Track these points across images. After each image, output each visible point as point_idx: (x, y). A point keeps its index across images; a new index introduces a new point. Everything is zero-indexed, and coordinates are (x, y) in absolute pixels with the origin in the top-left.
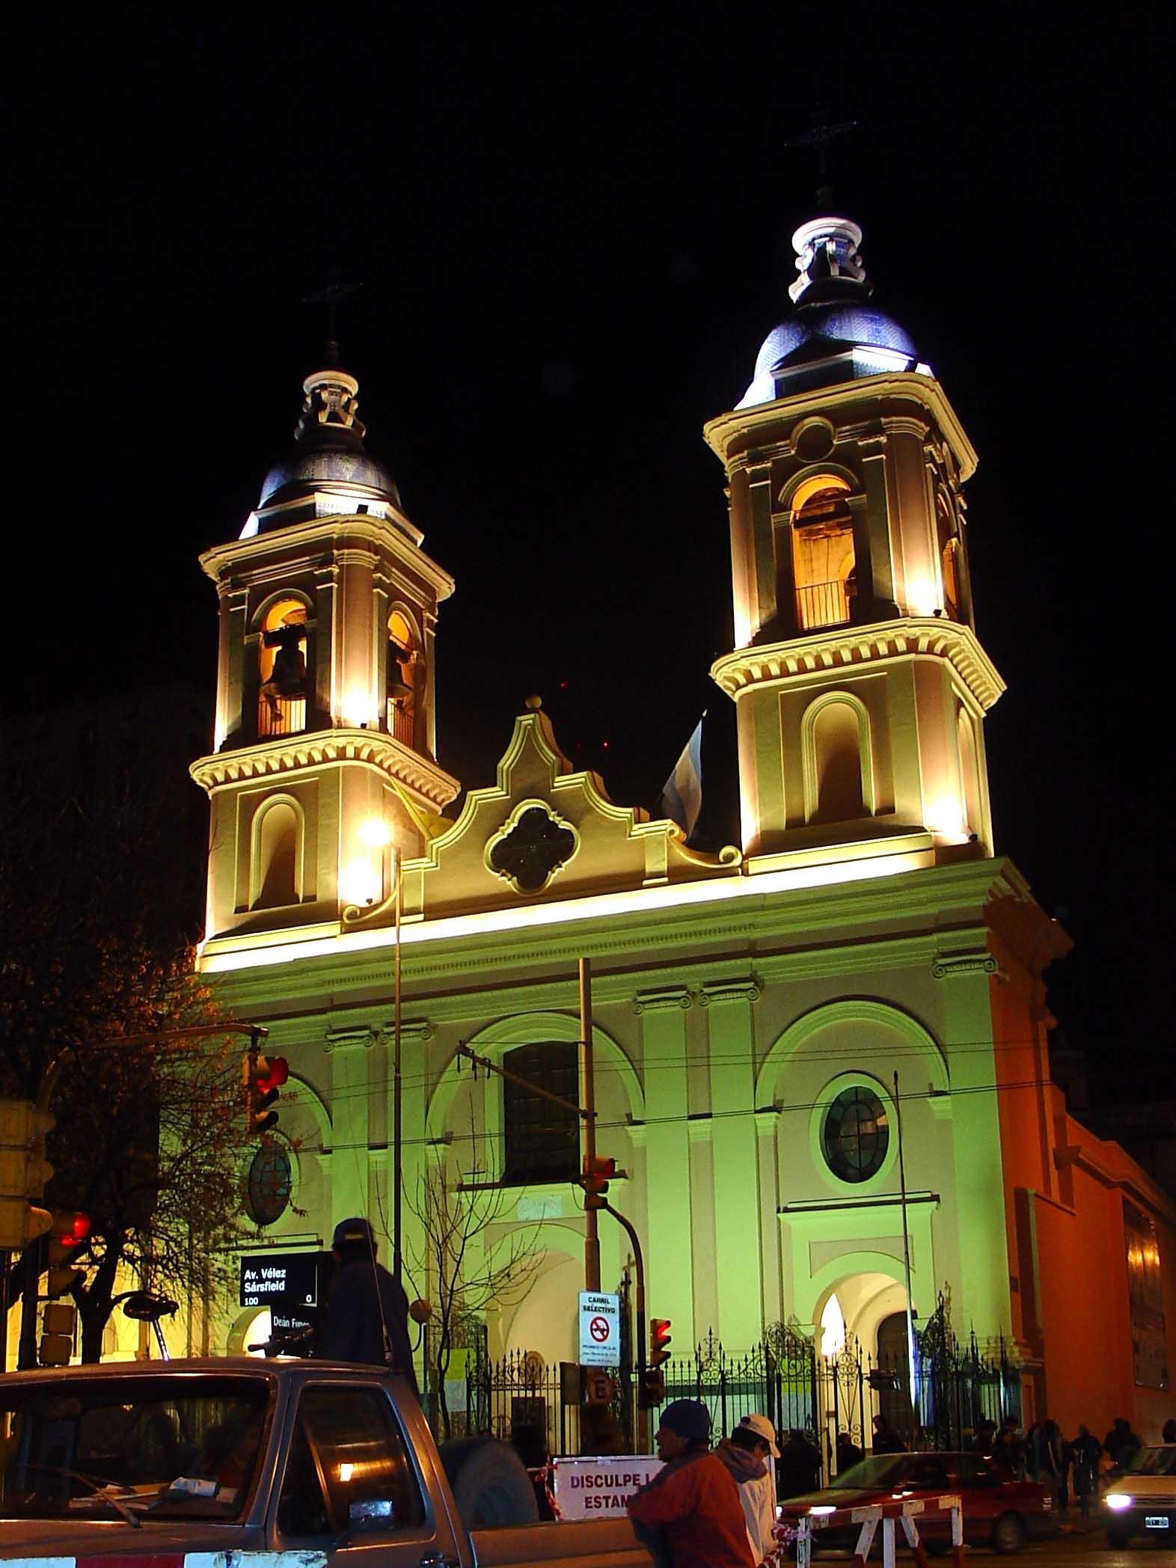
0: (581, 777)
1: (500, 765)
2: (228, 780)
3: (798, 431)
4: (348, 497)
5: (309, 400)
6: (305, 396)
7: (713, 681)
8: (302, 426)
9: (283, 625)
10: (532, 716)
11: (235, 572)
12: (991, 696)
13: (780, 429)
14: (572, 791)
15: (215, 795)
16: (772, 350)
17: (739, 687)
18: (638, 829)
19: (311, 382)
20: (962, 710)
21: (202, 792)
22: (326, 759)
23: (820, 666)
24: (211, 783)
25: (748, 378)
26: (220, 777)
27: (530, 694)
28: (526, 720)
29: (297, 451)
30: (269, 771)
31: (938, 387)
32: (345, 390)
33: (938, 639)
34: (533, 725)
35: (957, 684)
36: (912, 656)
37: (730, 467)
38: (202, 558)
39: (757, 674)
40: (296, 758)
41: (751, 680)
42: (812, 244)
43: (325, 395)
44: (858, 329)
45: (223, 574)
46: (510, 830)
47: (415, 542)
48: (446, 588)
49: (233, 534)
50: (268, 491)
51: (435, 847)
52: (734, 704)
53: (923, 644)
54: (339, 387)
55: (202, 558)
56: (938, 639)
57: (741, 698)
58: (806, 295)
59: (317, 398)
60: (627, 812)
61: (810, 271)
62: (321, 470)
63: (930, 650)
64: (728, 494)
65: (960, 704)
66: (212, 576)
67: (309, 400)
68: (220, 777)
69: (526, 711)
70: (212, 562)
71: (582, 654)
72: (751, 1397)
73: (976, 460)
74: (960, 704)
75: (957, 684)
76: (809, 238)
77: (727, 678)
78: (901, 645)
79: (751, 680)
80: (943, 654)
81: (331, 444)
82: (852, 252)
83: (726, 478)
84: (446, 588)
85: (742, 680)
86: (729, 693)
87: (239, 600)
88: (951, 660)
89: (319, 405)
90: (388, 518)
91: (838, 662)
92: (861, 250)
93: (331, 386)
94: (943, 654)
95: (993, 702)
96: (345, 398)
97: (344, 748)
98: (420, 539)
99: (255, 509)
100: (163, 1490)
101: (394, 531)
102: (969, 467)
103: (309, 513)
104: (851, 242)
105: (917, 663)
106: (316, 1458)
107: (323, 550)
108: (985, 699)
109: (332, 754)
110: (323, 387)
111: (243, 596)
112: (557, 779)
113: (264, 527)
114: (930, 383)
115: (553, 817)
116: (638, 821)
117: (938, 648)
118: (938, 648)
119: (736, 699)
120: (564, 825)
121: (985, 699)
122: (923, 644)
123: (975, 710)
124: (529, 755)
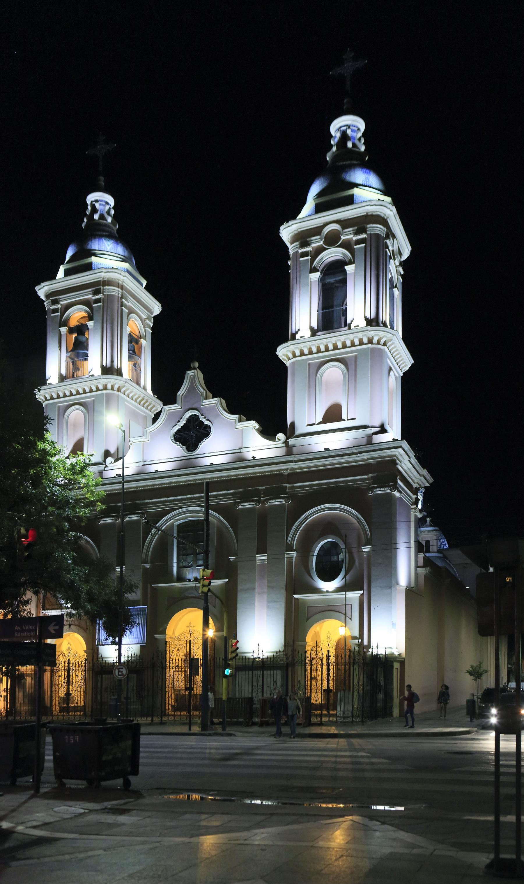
0: (215, 400)
1: (178, 394)
2: (52, 398)
3: (326, 230)
4: (110, 259)
5: (89, 207)
6: (88, 205)
7: (277, 356)
8: (85, 220)
9: (77, 324)
10: (193, 371)
11: (53, 295)
12: (406, 366)
13: (317, 231)
14: (210, 407)
15: (46, 405)
16: (315, 189)
17: (289, 359)
18: (240, 425)
19: (91, 198)
20: (392, 372)
21: (40, 404)
22: (98, 389)
23: (327, 349)
24: (44, 399)
25: (304, 202)
26: (48, 397)
27: (193, 361)
28: (190, 373)
29: (83, 233)
30: (71, 395)
31: (394, 209)
32: (107, 203)
33: (383, 337)
34: (194, 376)
35: (390, 360)
36: (370, 346)
37: (292, 248)
38: (37, 288)
39: (298, 353)
40: (97, 386)
41: (295, 356)
42: (338, 130)
43: (97, 205)
44: (359, 176)
45: (48, 296)
46: (182, 425)
47: (142, 285)
48: (157, 308)
49: (52, 276)
50: (69, 254)
51: (148, 431)
52: (287, 367)
53: (375, 340)
54: (104, 201)
55: (37, 288)
56: (383, 337)
57: (290, 364)
58: (335, 157)
59: (93, 207)
60: (236, 417)
61: (337, 145)
62: (96, 245)
63: (378, 343)
64: (289, 263)
65: (390, 369)
66: (43, 297)
67: (89, 207)
68: (48, 397)
69: (190, 369)
70: (42, 290)
71: (223, 341)
72: (279, 672)
73: (410, 249)
74: (390, 369)
75: (390, 360)
76: (338, 126)
77: (284, 355)
78: (365, 341)
79: (295, 356)
80: (385, 344)
81: (98, 230)
82: (360, 135)
83: (289, 255)
84: (157, 308)
85: (291, 356)
86: (285, 362)
87: (55, 311)
88: (388, 348)
89: (94, 210)
90: (128, 271)
91: (336, 348)
92: (364, 135)
93: (100, 201)
94: (385, 344)
95: (407, 368)
96: (107, 207)
97: (106, 385)
98: (145, 283)
99: (63, 264)
100: (174, 537)
101: (130, 278)
102: (406, 252)
103: (89, 267)
104: (359, 129)
105: (372, 349)
106: (236, 491)
107: (97, 287)
108: (403, 367)
109: (101, 387)
110: (97, 201)
111: (58, 308)
112: (204, 401)
113: (68, 273)
114: (390, 206)
115: (201, 419)
116: (240, 421)
117: (382, 342)
118: (382, 342)
119: (288, 365)
120: (206, 423)
121: (403, 367)
122: (375, 340)
123: (398, 373)
124: (192, 389)
